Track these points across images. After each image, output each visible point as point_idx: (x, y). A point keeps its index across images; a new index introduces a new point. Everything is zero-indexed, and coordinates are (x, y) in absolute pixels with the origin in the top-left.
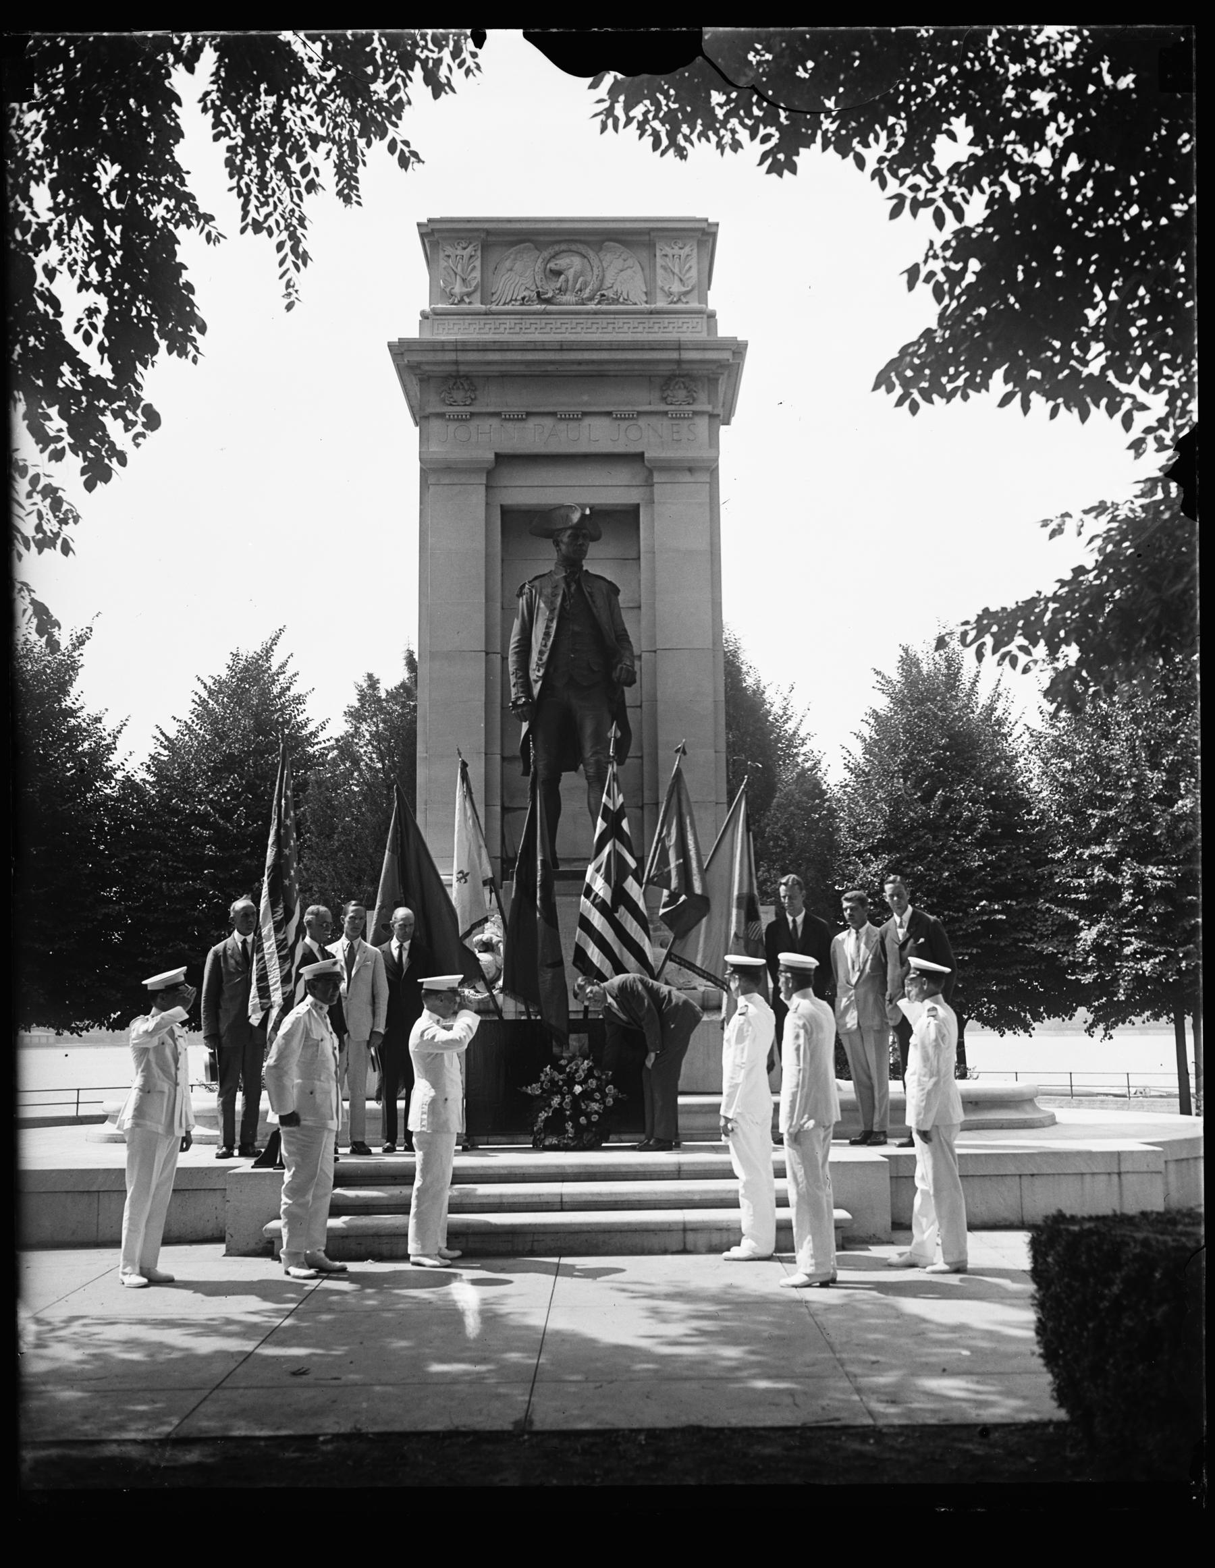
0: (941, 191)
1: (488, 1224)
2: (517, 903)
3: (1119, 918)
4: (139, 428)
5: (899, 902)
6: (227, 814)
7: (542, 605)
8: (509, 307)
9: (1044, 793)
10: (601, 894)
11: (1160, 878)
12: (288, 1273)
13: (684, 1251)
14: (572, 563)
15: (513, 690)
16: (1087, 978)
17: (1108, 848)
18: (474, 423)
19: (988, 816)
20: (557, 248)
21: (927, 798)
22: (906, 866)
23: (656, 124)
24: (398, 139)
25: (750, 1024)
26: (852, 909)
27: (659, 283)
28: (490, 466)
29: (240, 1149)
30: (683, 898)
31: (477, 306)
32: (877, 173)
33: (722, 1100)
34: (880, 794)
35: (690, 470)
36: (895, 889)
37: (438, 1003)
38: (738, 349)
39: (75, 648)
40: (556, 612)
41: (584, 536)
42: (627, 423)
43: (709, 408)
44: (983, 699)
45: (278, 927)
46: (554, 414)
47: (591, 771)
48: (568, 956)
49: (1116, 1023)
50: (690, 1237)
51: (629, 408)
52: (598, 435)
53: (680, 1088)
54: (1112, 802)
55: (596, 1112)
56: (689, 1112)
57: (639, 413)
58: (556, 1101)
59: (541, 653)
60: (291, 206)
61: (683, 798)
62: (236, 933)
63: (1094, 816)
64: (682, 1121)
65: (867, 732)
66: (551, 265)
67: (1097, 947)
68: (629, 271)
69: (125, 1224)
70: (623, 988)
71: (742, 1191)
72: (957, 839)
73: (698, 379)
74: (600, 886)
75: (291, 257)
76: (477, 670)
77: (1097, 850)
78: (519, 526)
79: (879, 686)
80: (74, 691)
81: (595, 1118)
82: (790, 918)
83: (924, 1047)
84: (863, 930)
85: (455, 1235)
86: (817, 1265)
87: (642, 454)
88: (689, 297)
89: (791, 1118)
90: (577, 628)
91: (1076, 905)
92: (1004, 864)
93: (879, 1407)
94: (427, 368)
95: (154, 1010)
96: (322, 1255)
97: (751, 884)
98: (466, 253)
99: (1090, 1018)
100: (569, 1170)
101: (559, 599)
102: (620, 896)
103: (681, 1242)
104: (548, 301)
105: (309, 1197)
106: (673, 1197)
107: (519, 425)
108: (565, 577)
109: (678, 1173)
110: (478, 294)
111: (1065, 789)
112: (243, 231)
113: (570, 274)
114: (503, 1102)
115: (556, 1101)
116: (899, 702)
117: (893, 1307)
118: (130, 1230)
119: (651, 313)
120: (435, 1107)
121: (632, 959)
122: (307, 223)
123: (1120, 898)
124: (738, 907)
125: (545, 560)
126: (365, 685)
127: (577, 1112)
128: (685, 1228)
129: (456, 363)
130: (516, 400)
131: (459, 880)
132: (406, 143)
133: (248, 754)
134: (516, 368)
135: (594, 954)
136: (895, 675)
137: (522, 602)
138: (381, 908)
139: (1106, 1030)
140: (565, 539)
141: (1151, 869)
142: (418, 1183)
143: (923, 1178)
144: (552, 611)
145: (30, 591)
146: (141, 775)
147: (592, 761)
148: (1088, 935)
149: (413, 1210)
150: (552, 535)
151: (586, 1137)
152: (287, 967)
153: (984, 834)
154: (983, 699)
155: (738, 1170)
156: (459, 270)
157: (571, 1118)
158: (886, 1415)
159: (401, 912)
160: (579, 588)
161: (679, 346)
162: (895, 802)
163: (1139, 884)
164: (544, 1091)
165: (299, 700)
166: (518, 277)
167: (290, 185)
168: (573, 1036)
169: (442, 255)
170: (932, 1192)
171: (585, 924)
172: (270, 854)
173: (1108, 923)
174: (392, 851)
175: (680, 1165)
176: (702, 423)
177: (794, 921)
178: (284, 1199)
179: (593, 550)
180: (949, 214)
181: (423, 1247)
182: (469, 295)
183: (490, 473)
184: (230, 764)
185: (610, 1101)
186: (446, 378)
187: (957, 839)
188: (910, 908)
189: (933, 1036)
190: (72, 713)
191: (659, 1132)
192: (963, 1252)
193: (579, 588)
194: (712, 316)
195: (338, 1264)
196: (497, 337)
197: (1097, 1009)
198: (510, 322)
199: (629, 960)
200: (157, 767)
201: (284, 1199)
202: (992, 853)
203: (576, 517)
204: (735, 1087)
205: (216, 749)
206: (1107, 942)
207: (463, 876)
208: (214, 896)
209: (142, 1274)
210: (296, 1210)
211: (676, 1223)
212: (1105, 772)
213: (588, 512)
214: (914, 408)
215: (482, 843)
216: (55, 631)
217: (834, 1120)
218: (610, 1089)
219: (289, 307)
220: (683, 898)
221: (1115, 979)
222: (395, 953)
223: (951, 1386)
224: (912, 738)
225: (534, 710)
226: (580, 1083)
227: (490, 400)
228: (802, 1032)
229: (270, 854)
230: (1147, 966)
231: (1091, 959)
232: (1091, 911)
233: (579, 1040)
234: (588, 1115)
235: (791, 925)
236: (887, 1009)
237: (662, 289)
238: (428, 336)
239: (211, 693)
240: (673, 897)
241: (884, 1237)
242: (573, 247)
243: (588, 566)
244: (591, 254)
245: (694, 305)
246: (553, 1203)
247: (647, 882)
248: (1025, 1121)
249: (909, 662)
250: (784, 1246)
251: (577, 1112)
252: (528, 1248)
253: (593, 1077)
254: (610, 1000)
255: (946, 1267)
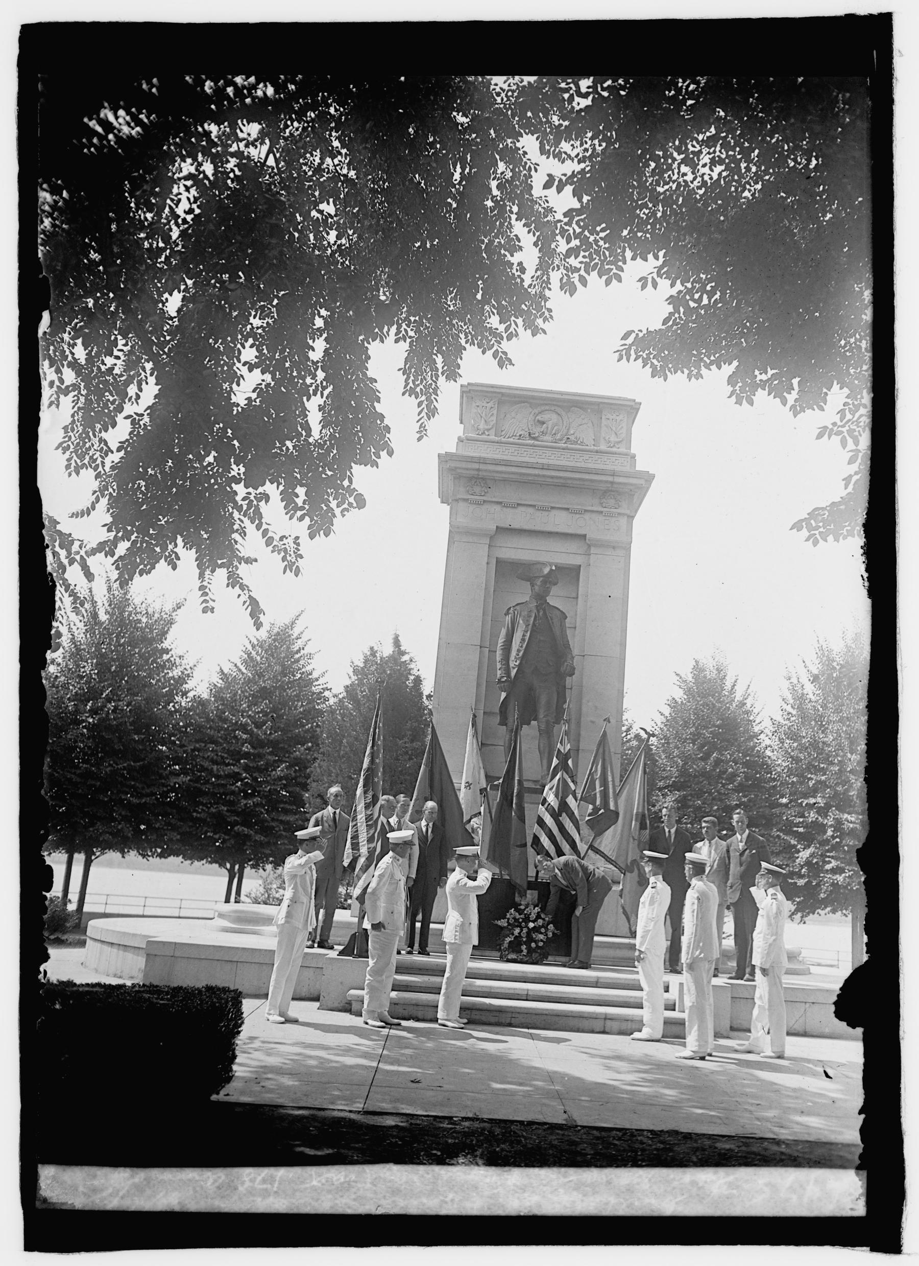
0: (847, 428)
1: (485, 1004)
2: (501, 806)
3: (824, 845)
4: (346, 506)
5: (742, 826)
6: (259, 725)
7: (521, 622)
8: (511, 440)
9: (780, 761)
10: (552, 804)
11: (851, 822)
12: (367, 1023)
13: (604, 1032)
14: (541, 598)
15: (499, 672)
16: (801, 882)
17: (819, 800)
18: (486, 506)
19: (744, 773)
20: (543, 408)
21: (705, 758)
22: (690, 800)
23: (655, 361)
24: (500, 350)
25: (658, 894)
26: (708, 828)
27: (603, 435)
28: (493, 533)
29: (319, 943)
30: (602, 811)
31: (492, 437)
32: (793, 407)
33: (637, 941)
34: (676, 752)
35: (614, 548)
36: (740, 818)
37: (466, 863)
38: (649, 478)
39: (174, 610)
40: (530, 627)
41: (550, 582)
42: (578, 516)
43: (628, 512)
44: (738, 697)
45: (367, 807)
46: (534, 506)
47: (543, 727)
48: (529, 840)
49: (808, 914)
50: (608, 1023)
51: (579, 507)
52: (559, 522)
53: (596, 932)
54: (824, 771)
55: (542, 941)
56: (600, 947)
57: (586, 511)
58: (517, 931)
59: (519, 651)
60: (430, 382)
61: (606, 749)
62: (329, 807)
63: (812, 779)
64: (596, 952)
65: (667, 711)
66: (539, 418)
67: (808, 863)
68: (585, 426)
69: (272, 983)
70: (566, 864)
71: (645, 997)
72: (723, 785)
73: (615, 492)
74: (551, 799)
75: (425, 410)
76: (474, 657)
77: (812, 801)
78: (507, 571)
79: (678, 683)
80: (170, 636)
81: (541, 944)
82: (667, 830)
83: (768, 917)
84: (713, 842)
85: (465, 1009)
86: (699, 1045)
87: (585, 536)
88: (619, 445)
89: (688, 953)
90: (542, 638)
91: (797, 835)
92: (751, 804)
93: (776, 1129)
94: (459, 471)
95: (300, 852)
96: (386, 1013)
97: (644, 806)
98: (489, 405)
99: (793, 908)
100: (530, 975)
101: (532, 619)
102: (564, 806)
103: (602, 1027)
104: (534, 439)
105: (384, 977)
106: (597, 998)
107: (514, 510)
108: (537, 606)
109: (596, 984)
110: (493, 430)
111: (793, 760)
112: (403, 394)
113: (550, 423)
114: (498, 929)
115: (517, 931)
116: (688, 692)
117: (752, 1075)
118: (275, 987)
119: (597, 452)
120: (463, 928)
121: (568, 846)
122: (439, 392)
123: (826, 832)
124: (636, 820)
125: (522, 594)
126: (369, 653)
127: (530, 939)
128: (606, 1018)
129: (478, 470)
130: (511, 495)
131: (466, 787)
132: (505, 353)
133: (275, 688)
134: (511, 476)
135: (545, 841)
136: (690, 678)
137: (508, 619)
138: (416, 800)
139: (802, 917)
140: (539, 583)
141: (846, 816)
142: (447, 975)
143: (761, 998)
144: (527, 626)
145: (249, 590)
146: (205, 696)
147: (544, 720)
148: (804, 855)
149: (443, 991)
150: (531, 580)
151: (535, 956)
152: (372, 832)
153: (740, 784)
154: (738, 697)
155: (644, 984)
156: (483, 415)
157: (525, 943)
158: (783, 1134)
159: (430, 804)
160: (545, 613)
161: (614, 474)
162: (686, 759)
163: (839, 823)
164: (509, 924)
165: (310, 656)
166: (519, 422)
167: (432, 370)
168: (529, 892)
169: (474, 405)
170: (767, 1007)
171: (541, 822)
172: (366, 761)
173: (816, 848)
174: (426, 765)
175: (598, 978)
176: (623, 521)
177: (669, 832)
178: (368, 977)
179: (554, 590)
180: (850, 441)
181: (447, 1015)
182: (488, 430)
183: (491, 538)
184: (264, 693)
185: (550, 935)
186: (471, 478)
187: (723, 785)
188: (747, 831)
189: (774, 911)
190: (167, 651)
191: (581, 957)
192: (783, 1046)
193: (545, 613)
194: (633, 457)
195: (396, 1021)
196: (505, 458)
197: (798, 903)
198: (512, 449)
199: (566, 847)
200: (217, 693)
201: (368, 977)
202: (745, 796)
203: (546, 570)
204: (647, 932)
205: (255, 683)
206: (815, 860)
207: (468, 785)
208: (246, 778)
209: (280, 1015)
210: (376, 984)
211: (601, 1014)
212: (821, 752)
213: (554, 568)
214: (815, 543)
215: (481, 765)
216: (261, 616)
217: (715, 957)
218: (551, 927)
219: (419, 439)
220: (602, 811)
221: (818, 885)
222: (424, 829)
223: (813, 1121)
224: (697, 719)
225: (511, 685)
226: (533, 922)
227: (496, 494)
228: (696, 901)
229: (366, 761)
230: (840, 878)
231: (804, 870)
232: (806, 839)
233: (532, 895)
234: (536, 942)
235: (667, 834)
236: (728, 892)
237: (604, 438)
238: (460, 452)
239: (253, 647)
240: (596, 810)
241: (725, 1034)
242: (553, 408)
243: (551, 601)
244: (563, 413)
245: (623, 450)
246: (522, 995)
247: (581, 800)
248: (795, 969)
249: (698, 669)
250: (674, 1031)
251: (530, 939)
252: (508, 1021)
253: (541, 918)
254: (557, 871)
255: (773, 1055)
